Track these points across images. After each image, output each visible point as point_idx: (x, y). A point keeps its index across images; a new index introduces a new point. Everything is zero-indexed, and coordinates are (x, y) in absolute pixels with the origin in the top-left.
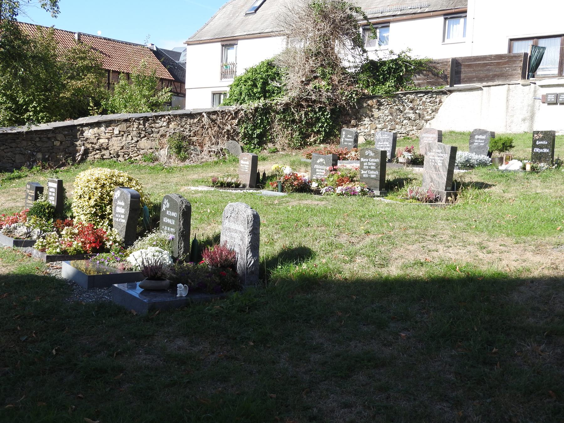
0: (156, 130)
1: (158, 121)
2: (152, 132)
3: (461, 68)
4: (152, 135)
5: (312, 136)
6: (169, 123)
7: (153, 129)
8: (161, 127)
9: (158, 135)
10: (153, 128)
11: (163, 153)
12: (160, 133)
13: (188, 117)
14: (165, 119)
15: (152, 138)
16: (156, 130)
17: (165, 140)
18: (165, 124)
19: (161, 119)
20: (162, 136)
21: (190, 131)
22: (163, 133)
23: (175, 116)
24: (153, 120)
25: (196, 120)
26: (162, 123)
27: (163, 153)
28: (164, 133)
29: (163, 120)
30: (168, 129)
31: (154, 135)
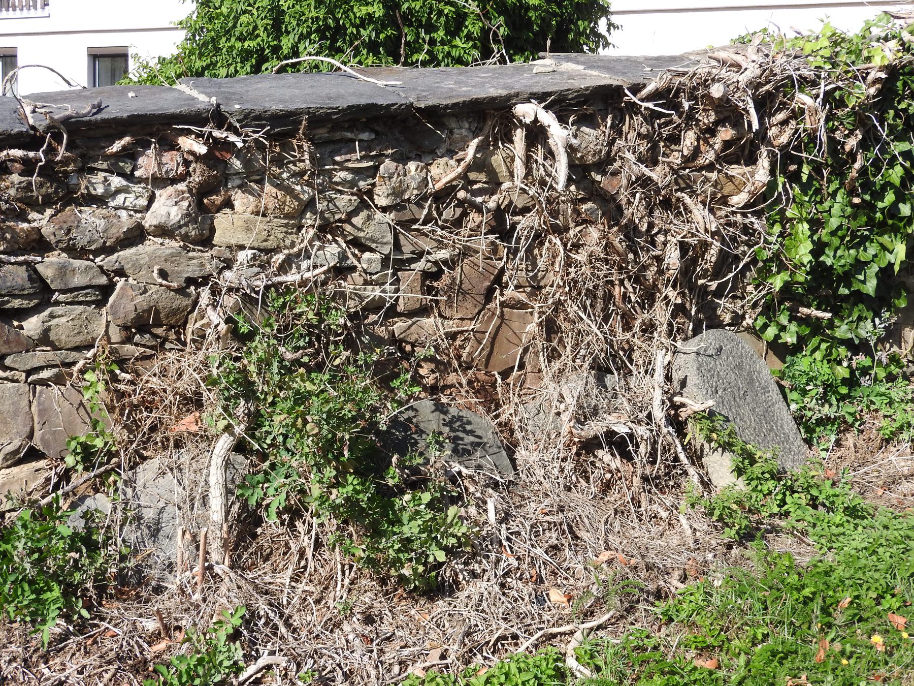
0: (82, 272)
1: (98, 184)
2: (42, 294)
3: (142, 154)
4: (32, 325)
5: (897, 268)
6: (205, 204)
7: (49, 265)
8: (136, 235)
9: (103, 324)
10: (40, 245)
11: (183, 494)
12: (126, 300)
13: (381, 140)
14: (171, 162)
15: (41, 356)
16: (82, 272)
17: (181, 368)
18: (168, 207)
19: (130, 154)
20: (139, 325)
21: (396, 263)
22: (160, 296)
23: (282, 126)
24: (49, 172)
25: (444, 172)
26: (135, 197)
27: (183, 494)
28: (167, 300)
29: (147, 164)
30: (200, 261)
31: (64, 321)
